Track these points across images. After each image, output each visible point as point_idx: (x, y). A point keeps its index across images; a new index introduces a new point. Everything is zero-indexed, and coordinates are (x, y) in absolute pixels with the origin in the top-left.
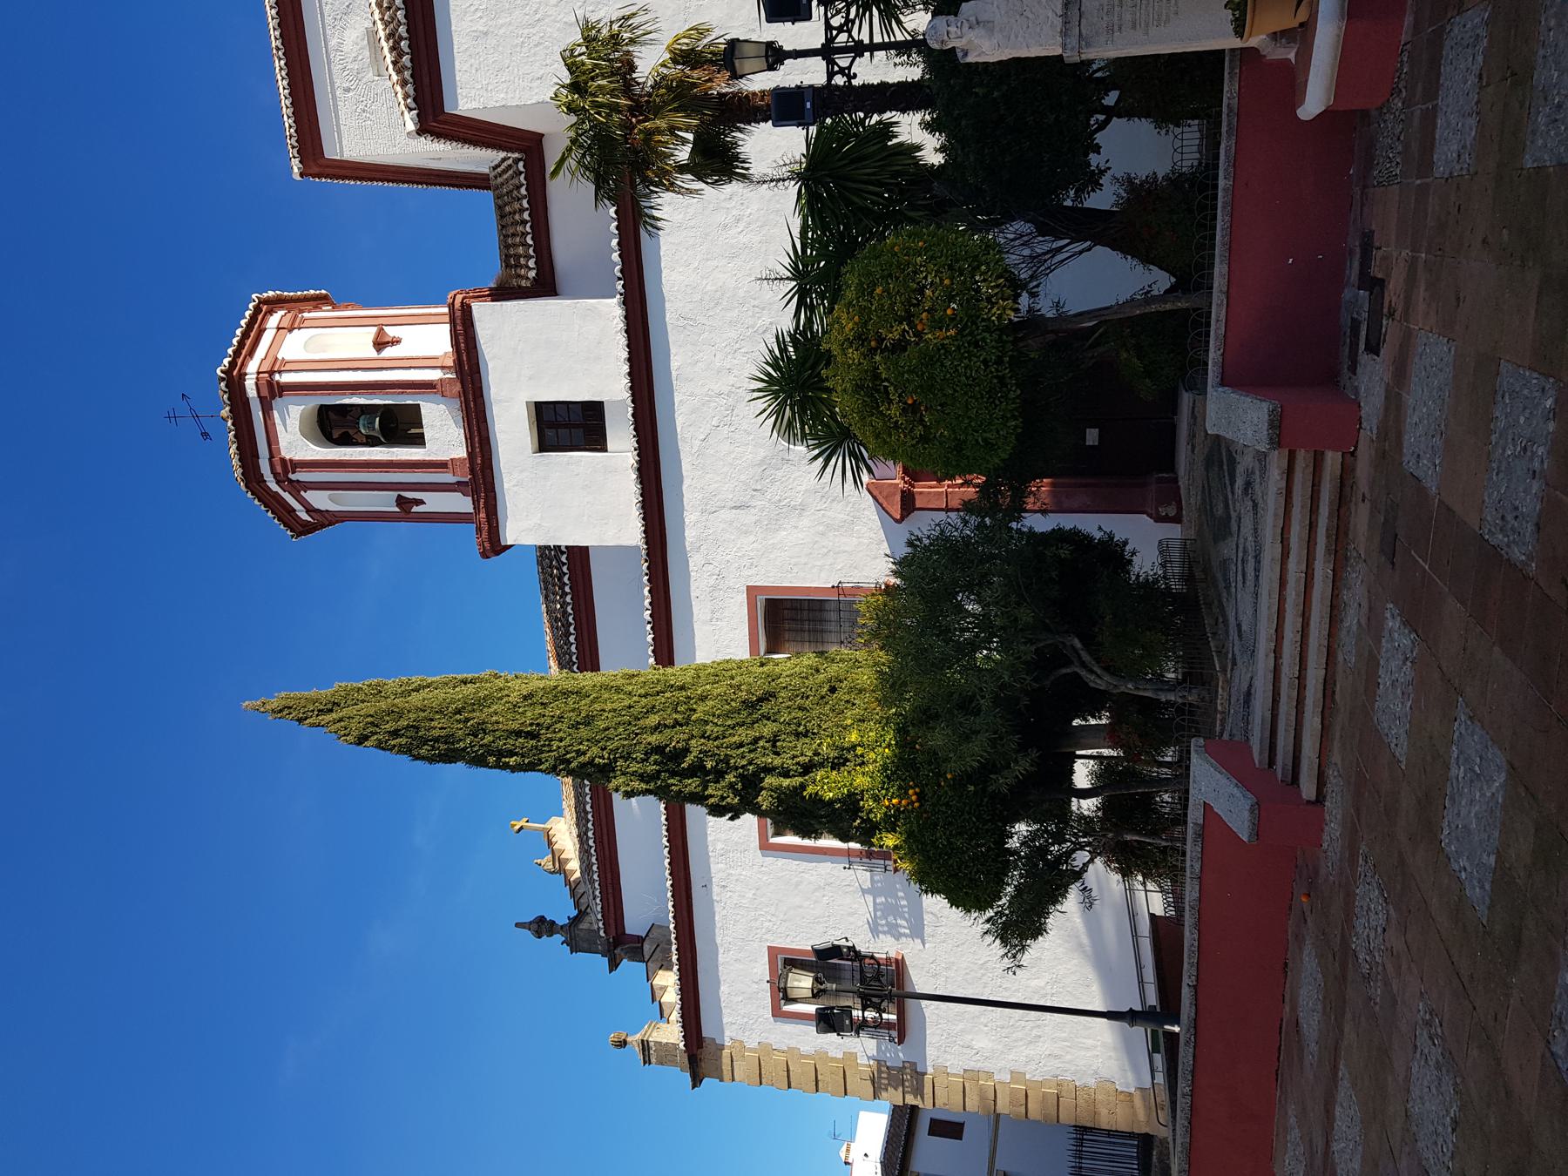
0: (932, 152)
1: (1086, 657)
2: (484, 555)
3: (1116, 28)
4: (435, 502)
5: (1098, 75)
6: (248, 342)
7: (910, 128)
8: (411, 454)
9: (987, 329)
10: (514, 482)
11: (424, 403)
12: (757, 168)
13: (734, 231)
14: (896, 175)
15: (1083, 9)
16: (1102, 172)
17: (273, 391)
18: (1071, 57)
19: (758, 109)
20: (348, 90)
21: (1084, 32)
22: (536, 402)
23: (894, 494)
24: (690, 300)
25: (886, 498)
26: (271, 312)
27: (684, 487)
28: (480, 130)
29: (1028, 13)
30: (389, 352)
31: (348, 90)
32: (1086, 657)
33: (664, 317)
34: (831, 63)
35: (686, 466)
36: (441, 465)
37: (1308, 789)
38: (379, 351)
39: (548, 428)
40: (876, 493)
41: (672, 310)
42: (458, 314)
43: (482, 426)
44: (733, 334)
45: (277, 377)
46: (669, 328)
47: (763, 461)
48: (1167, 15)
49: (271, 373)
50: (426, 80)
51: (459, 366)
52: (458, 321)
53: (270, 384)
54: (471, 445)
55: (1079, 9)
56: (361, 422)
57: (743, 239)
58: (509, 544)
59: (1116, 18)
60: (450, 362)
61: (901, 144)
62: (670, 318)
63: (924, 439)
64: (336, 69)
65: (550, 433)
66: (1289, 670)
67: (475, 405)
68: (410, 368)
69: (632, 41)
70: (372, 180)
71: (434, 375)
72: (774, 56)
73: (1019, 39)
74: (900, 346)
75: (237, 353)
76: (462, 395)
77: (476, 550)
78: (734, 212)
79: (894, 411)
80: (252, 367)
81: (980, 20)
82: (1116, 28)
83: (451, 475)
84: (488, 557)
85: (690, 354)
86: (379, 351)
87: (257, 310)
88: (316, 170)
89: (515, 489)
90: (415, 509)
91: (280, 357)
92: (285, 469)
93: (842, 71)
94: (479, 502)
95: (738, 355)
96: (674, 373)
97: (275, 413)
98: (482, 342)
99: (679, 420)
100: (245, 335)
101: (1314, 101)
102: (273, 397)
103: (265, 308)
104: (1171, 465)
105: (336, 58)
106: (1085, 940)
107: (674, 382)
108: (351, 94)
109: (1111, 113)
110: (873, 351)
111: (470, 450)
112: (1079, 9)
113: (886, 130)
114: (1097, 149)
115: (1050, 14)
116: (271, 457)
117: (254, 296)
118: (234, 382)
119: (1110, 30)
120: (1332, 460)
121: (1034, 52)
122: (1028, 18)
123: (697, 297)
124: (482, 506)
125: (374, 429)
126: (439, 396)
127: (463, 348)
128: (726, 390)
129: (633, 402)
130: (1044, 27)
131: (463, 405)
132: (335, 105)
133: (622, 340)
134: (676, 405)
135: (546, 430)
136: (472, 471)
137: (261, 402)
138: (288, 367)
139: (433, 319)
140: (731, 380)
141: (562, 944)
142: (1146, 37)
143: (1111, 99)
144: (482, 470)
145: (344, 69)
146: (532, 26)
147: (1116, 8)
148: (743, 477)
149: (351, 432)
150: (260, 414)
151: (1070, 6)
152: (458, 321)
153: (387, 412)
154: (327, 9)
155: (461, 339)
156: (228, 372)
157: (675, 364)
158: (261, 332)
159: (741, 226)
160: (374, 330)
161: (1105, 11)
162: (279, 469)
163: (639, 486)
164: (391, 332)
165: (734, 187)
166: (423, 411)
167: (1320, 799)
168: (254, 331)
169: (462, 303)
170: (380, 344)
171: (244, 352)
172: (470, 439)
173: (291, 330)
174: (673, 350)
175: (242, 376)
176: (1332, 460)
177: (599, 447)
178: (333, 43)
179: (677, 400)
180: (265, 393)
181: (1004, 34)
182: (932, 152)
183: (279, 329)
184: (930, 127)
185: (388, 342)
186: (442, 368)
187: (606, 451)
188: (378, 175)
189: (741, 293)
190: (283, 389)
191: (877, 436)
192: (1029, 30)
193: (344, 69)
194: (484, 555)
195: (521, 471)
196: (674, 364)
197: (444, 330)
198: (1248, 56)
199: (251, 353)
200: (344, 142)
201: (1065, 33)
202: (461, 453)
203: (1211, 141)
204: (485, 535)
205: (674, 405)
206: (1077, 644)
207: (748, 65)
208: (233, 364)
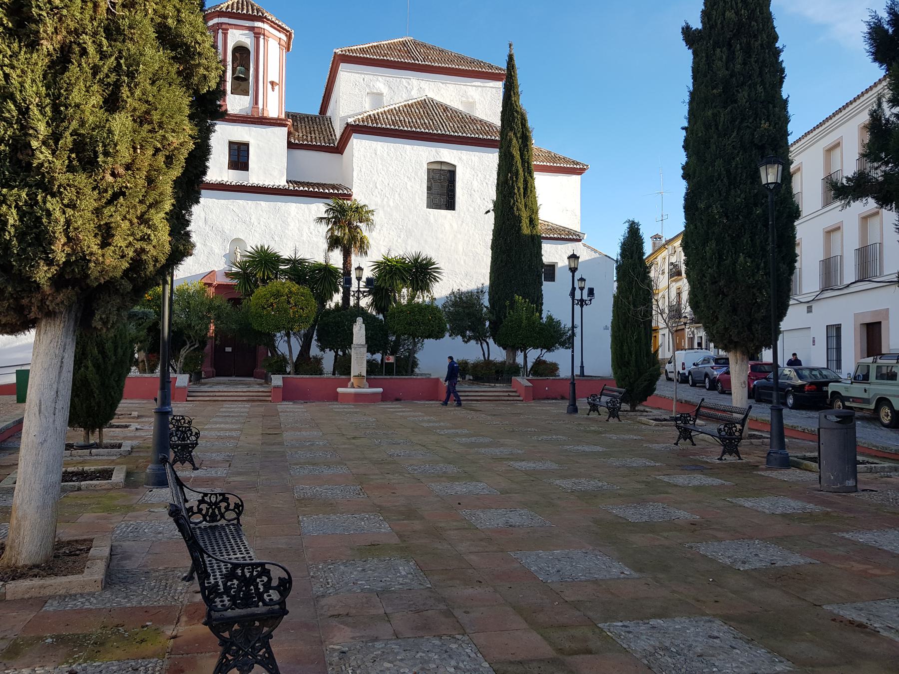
0: (331, 304)
1: (192, 348)
5: (347, 352)
6: (276, 26)
7: (337, 298)
9: (292, 325)
12: (331, 254)
13: (307, 231)
14: (325, 294)
16: (324, 352)
17: (257, 34)
18: (353, 346)
19: (347, 259)
20: (364, 80)
23: (211, 281)
25: (209, 277)
26: (286, 35)
27: (214, 200)
28: (346, 140)
30: (269, 86)
31: (364, 80)
32: (192, 348)
34: (356, 292)
35: (223, 201)
37: (189, 399)
38: (270, 82)
40: (212, 274)
42: (284, 122)
44: (272, 226)
45: (262, 37)
47: (224, 231)
49: (264, 35)
50: (364, 129)
53: (259, 34)
56: (242, 68)
57: (305, 234)
61: (333, 295)
63: (264, 308)
64: (371, 77)
65: (236, 147)
66: (217, 394)
69: (368, 224)
70: (330, 72)
71: (260, 106)
72: (359, 279)
74: (289, 302)
75: (272, 22)
78: (313, 233)
79: (272, 301)
80: (266, 26)
86: (270, 82)
87: (288, 31)
88: (337, 58)
91: (269, 39)
92: (224, 29)
93: (354, 294)
95: (264, 227)
96: (259, 202)
97: (247, 32)
99: (241, 202)
100: (279, 26)
101: (340, 390)
102: (255, 33)
103: (288, 34)
104: (218, 375)
105: (375, 78)
106: (7, 347)
108: (362, 81)
109: (336, 353)
110: (287, 296)
113: (337, 291)
114: (330, 350)
116: (229, 24)
117: (293, 31)
118: (262, 19)
119: (357, 353)
120: (270, 399)
121: (354, 339)
123: (286, 215)
125: (240, 73)
126: (252, 105)
128: (252, 221)
132: (359, 73)
137: (252, 27)
138: (266, 42)
139: (280, 105)
140: (256, 224)
143: (340, 353)
145: (371, 80)
146: (377, 171)
148: (218, 223)
149: (238, 62)
150: (247, 25)
153: (246, 79)
154: (391, 79)
156: (265, 17)
158: (279, 31)
159: (309, 234)
160: (278, 82)
162: (224, 26)
164: (277, 88)
165: (326, 246)
167: (187, 401)
168: (280, 29)
170: (272, 83)
171: (272, 24)
172: (235, 116)
173: (279, 44)
174: (267, 203)
175: (263, 22)
176: (270, 399)
178: (380, 78)
179: (249, 202)
180: (256, 30)
182: (331, 304)
183: (280, 39)
184: (337, 304)
186: (263, 108)
188: (331, 78)
189: (287, 231)
190: (257, 39)
191: (265, 295)
193: (371, 80)
195: (221, 134)
196: (262, 203)
197: (276, 116)
198: (350, 379)
199: (271, 26)
200: (346, 73)
201: (357, 345)
203: (184, 506)
206: (196, 346)
207: (358, 272)
208: (268, 20)
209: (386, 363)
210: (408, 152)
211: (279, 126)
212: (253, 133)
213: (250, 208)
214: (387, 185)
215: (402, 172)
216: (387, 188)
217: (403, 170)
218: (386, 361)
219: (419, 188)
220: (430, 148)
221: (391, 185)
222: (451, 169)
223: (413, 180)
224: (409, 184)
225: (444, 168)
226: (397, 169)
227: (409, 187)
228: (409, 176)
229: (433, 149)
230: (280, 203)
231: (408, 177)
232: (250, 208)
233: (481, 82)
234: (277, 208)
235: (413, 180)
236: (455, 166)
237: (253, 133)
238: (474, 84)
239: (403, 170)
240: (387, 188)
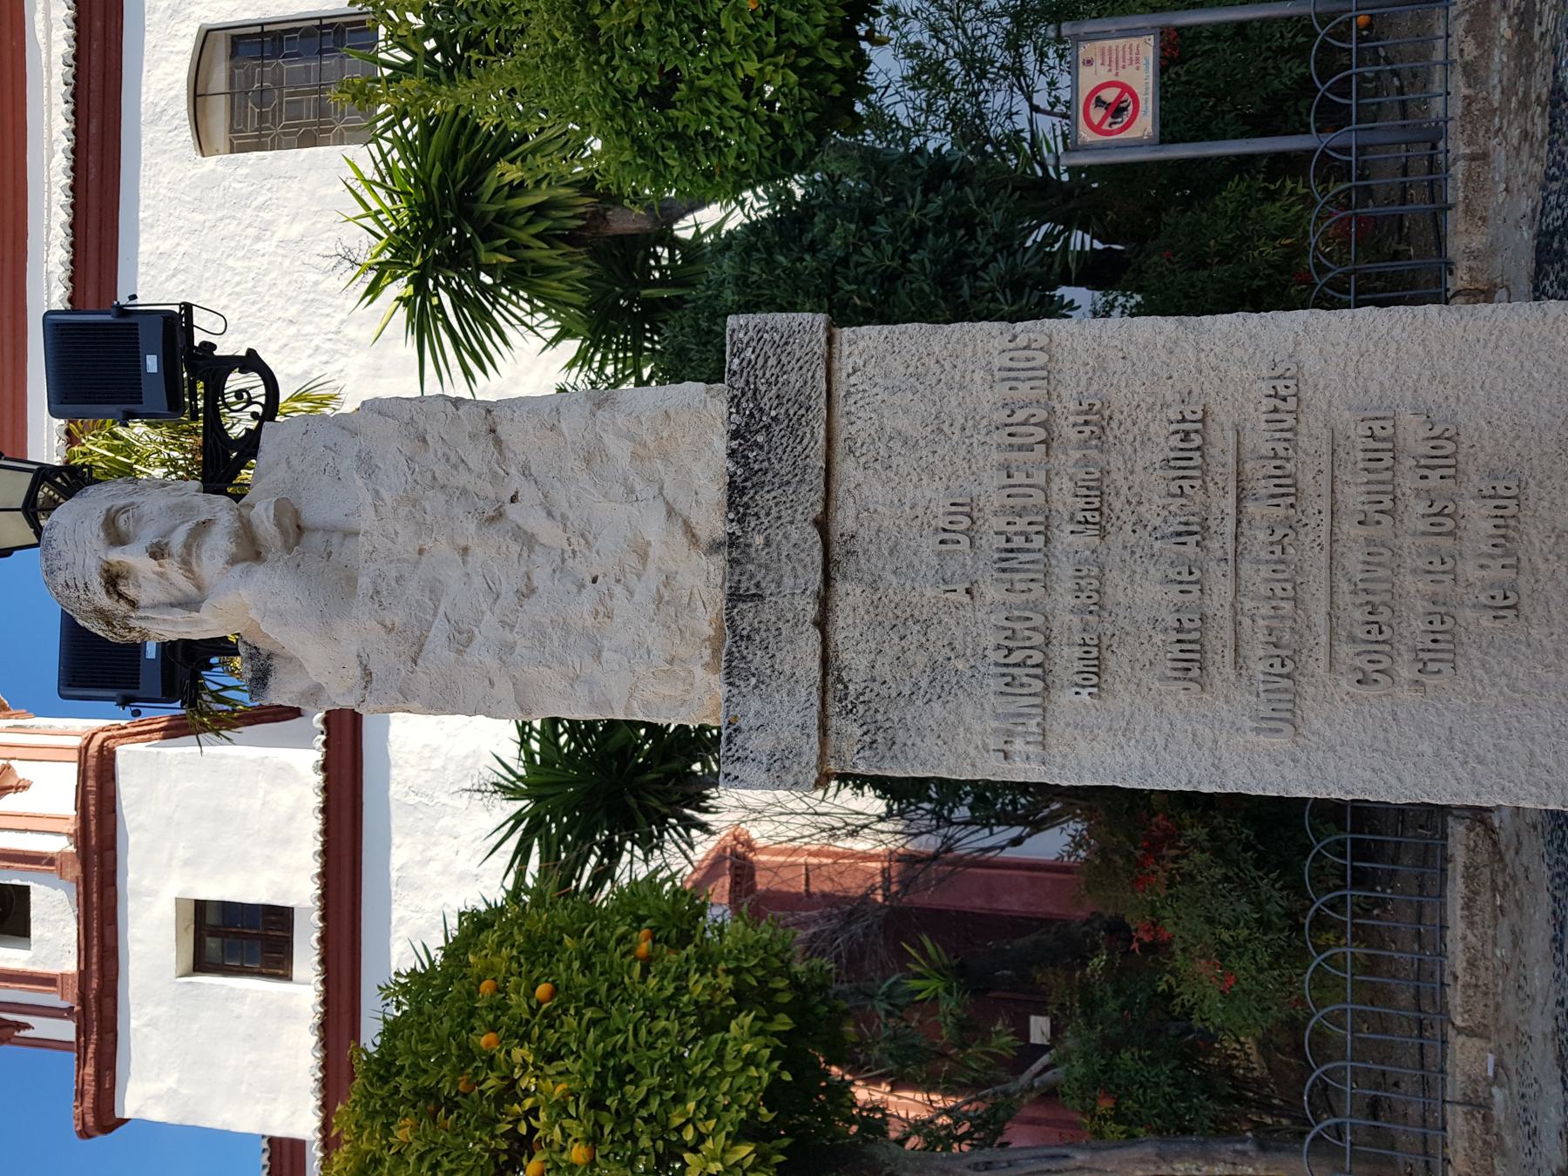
2: (85, 1134)
3: (1067, 658)
4: (43, 1028)
8: (9, 960)
10: (144, 1020)
11: (37, 885)
15: (845, 520)
21: (854, 660)
22: (196, 901)
24: (425, 767)
29: (528, 516)
33: (387, 789)
36: (48, 981)
39: (210, 936)
41: (400, 779)
42: (92, 762)
43: (108, 931)
46: (393, 807)
48: (1441, 614)
51: (82, 837)
52: (91, 773)
54: (86, 960)
55: (822, 525)
58: (126, 1117)
59: (1064, 597)
60: (71, 827)
62: (395, 791)
65: (212, 944)
67: (101, 897)
68: (26, 831)
73: (476, 654)
76: (81, 882)
77: (74, 1126)
81: (310, 516)
82: (1067, 658)
83: (59, 997)
84: (89, 1137)
85: (421, 848)
89: (145, 1030)
90: (23, 1033)
94: (86, 1049)
96: (394, 875)
98: (124, 803)
107: (394, 889)
111: (82, 967)
112: (822, 525)
115: (654, 527)
122: (528, 540)
123: (437, 763)
124: (90, 1055)
126: (56, 877)
127: (92, 813)
129: (323, 918)
130: (620, 601)
131: (81, 898)
133: (315, 824)
134: (393, 924)
135: (208, 939)
136: (83, 998)
141: (1079, 307)
142: (1281, 742)
144: (99, 1000)
147: (1064, 537)
151: (765, 498)
152: (91, 773)
155: (92, 799)
157: (398, 857)
161: (991, 543)
163: (318, 1055)
166: (33, 897)
169: (101, 746)
174: (396, 839)
177: (281, 972)
179: (395, 916)
181: (397, 617)
185: (11, 787)
187: (290, 979)
192: (533, 608)
194: (85, 1134)
195: (158, 1004)
202: (70, 965)
204: (88, 1102)
205: (390, 923)
209: (1168, 131)
210: (165, 246)
211: (113, 778)
212: (146, 882)
213: (418, 910)
214: (293, 330)
215: (238, 265)
216: (308, 329)
217: (230, 262)
218: (1144, 125)
219: (295, 185)
220: (145, 153)
221: (292, 312)
222: (221, 49)
223: (266, 216)
224: (281, 232)
225: (219, 78)
226: (228, 290)
227: (296, 230)
228: (252, 231)
229: (147, 134)
230: (393, 788)
231: (258, 238)
232: (418, 910)
233: (34, 10)
234: (412, 799)
235: (266, 216)
236: (207, 36)
237: (146, 882)
238: (40, 36)
239: (230, 262)
240: (308, 329)
